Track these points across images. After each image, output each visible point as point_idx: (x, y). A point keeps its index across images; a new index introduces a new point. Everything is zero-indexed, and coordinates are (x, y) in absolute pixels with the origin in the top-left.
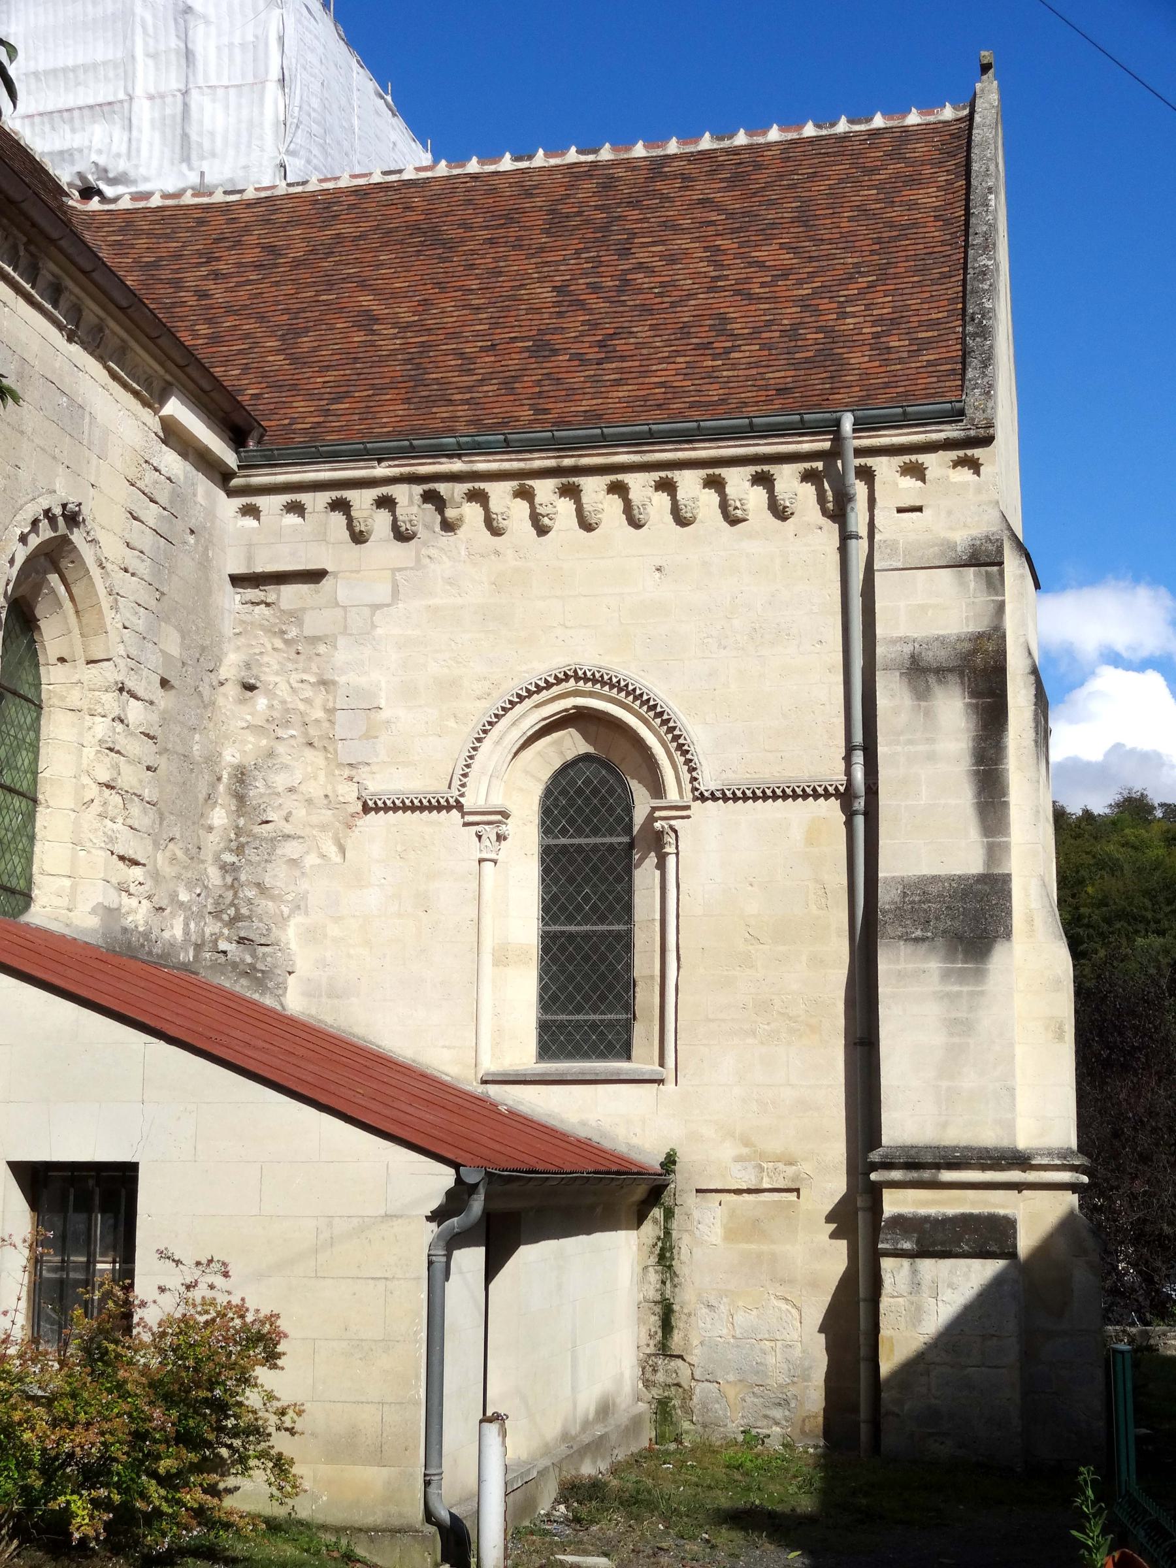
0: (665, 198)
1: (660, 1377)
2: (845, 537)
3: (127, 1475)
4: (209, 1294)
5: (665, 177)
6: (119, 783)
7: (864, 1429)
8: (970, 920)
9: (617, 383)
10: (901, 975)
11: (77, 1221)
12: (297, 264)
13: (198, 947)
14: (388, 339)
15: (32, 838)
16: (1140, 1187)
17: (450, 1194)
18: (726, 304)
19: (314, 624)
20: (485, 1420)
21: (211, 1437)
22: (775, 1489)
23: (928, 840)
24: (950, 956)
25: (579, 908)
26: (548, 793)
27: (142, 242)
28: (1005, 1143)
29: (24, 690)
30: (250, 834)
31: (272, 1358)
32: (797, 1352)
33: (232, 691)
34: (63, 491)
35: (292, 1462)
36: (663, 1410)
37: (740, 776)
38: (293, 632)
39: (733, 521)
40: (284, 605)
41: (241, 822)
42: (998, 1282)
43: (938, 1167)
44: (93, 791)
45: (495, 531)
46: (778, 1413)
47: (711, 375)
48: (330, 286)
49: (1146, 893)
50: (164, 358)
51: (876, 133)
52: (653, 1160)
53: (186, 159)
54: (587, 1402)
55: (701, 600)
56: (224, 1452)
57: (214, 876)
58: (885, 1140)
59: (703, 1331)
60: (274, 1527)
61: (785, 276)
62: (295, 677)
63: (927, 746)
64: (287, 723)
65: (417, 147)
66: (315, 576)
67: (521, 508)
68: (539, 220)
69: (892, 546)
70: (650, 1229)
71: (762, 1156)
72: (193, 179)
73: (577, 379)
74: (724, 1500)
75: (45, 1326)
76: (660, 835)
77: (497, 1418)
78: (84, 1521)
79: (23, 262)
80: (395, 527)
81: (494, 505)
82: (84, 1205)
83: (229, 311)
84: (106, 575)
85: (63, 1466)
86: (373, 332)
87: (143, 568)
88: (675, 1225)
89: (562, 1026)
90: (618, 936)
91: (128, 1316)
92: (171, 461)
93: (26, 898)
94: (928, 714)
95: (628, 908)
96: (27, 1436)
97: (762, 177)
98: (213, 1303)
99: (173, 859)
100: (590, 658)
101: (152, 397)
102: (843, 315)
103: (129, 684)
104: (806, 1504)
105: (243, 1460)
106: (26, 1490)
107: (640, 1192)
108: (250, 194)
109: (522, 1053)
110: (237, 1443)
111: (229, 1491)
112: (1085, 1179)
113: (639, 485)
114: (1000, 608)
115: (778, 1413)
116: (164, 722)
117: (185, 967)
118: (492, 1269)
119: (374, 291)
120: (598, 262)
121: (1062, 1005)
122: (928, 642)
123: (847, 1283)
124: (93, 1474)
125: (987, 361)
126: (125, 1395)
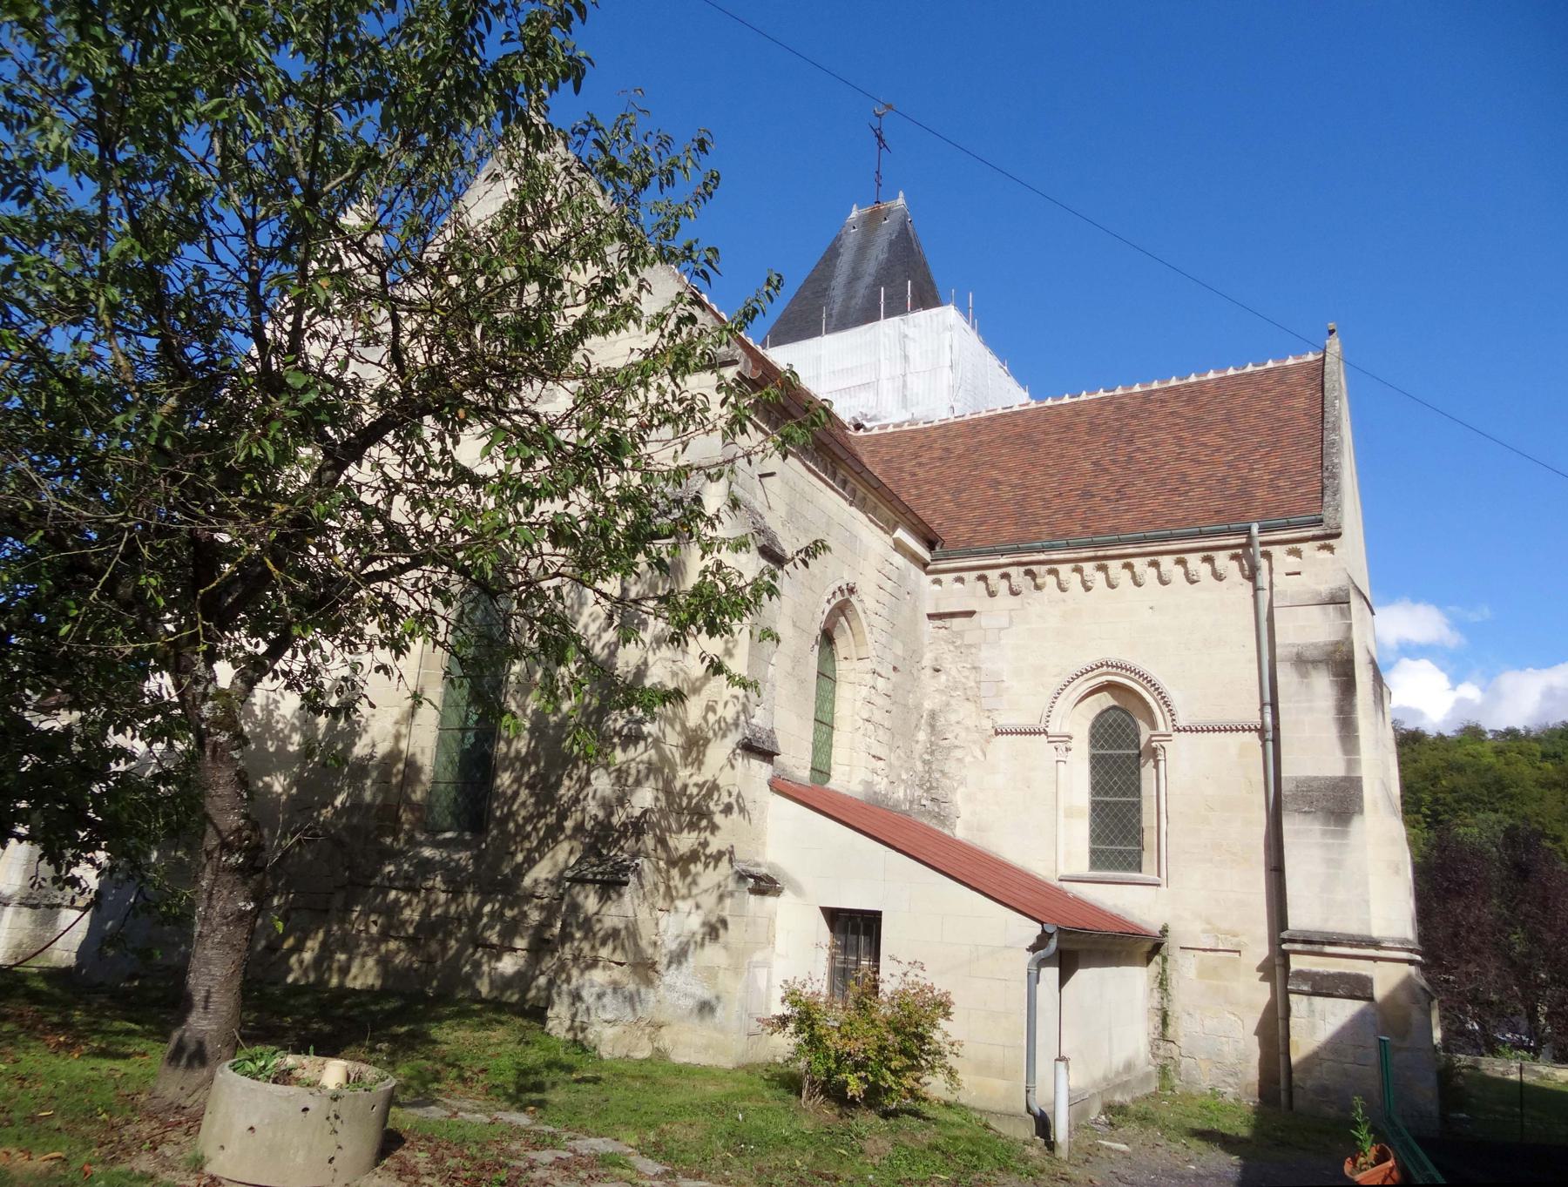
11: (852, 938)
12: (960, 457)
13: (911, 802)
14: (1006, 493)
27: (884, 450)
31: (947, 1015)
33: (928, 672)
38: (959, 643)
48: (976, 467)
50: (895, 510)
57: (919, 766)
64: (956, 689)
72: (908, 417)
78: (855, 1087)
92: (898, 559)
101: (889, 528)
103: (878, 670)
105: (932, 1068)
106: (828, 1069)
108: (936, 423)
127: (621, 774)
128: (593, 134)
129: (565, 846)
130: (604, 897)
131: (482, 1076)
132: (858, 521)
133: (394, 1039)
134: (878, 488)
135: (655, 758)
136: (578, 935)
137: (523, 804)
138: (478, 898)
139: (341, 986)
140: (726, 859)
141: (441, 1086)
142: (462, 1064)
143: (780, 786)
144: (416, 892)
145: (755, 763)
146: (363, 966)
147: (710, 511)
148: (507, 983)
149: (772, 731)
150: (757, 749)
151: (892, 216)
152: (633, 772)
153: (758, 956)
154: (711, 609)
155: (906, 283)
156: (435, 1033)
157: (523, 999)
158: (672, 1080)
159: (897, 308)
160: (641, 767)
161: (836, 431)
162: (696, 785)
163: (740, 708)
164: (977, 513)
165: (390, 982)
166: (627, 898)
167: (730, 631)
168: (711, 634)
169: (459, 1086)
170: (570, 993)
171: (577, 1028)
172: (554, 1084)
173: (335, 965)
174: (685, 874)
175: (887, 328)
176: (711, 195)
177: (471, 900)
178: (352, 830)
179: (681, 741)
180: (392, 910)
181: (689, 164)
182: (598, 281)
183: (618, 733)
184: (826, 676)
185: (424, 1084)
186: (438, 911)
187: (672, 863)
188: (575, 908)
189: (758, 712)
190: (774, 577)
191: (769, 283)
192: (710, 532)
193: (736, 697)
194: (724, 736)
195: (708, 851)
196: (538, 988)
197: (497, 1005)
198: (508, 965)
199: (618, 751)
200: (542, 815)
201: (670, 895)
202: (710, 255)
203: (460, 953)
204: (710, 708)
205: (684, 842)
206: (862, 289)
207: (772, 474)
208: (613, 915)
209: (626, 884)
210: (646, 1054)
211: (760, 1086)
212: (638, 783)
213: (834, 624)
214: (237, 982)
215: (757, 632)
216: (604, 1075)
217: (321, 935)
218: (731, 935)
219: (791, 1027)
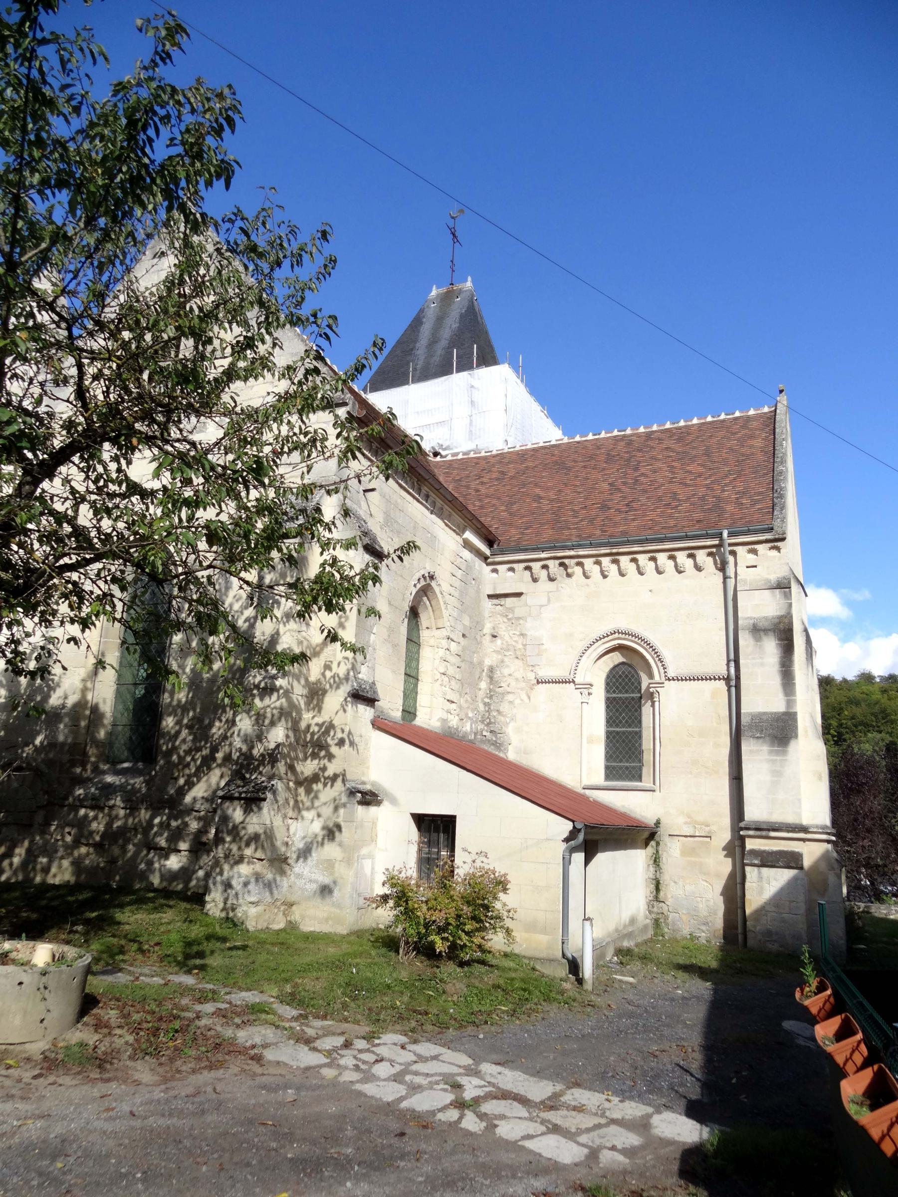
0: (653, 447)
1: (655, 910)
2: (725, 578)
5: (652, 439)
6: (448, 673)
7: (740, 937)
8: (781, 731)
9: (634, 520)
10: (751, 751)
12: (512, 478)
13: (476, 734)
14: (545, 505)
16: (866, 843)
17: (571, 832)
18: (676, 488)
19: (518, 612)
20: (585, 919)
22: (703, 958)
23: (762, 696)
24: (772, 744)
25: (621, 722)
26: (608, 677)
27: (455, 472)
28: (797, 822)
31: (505, 890)
32: (711, 903)
33: (488, 638)
34: (429, 568)
36: (657, 923)
37: (684, 671)
39: (680, 572)
42: (794, 879)
43: (769, 830)
44: (438, 676)
45: (587, 577)
46: (704, 928)
47: (670, 516)
48: (524, 485)
49: (872, 714)
50: (464, 517)
51: (736, 419)
52: (651, 822)
53: (471, 439)
54: (625, 917)
55: (669, 603)
57: (481, 707)
58: (746, 818)
59: (673, 891)
60: (506, 955)
61: (700, 476)
63: (760, 663)
64: (508, 650)
66: (519, 595)
67: (597, 568)
68: (603, 458)
69: (745, 581)
70: (650, 850)
71: (696, 822)
72: (473, 447)
73: (617, 519)
74: (681, 961)
76: (652, 694)
77: (589, 919)
78: (440, 946)
81: (586, 567)
82: (437, 830)
83: (487, 496)
84: (443, 597)
88: (660, 848)
89: (614, 768)
90: (636, 733)
91: (453, 871)
92: (467, 554)
93: (415, 715)
94: (760, 647)
95: (640, 722)
97: (690, 438)
100: (624, 626)
101: (460, 531)
102: (724, 491)
104: (714, 964)
106: (419, 933)
107: (646, 835)
108: (494, 453)
109: (599, 777)
112: (834, 838)
113: (642, 559)
114: (790, 605)
115: (704, 928)
117: (471, 741)
118: (587, 862)
119: (540, 487)
120: (626, 474)
121: (823, 768)
122: (760, 619)
123: (732, 876)
124: (441, 930)
125: (783, 507)
126: (453, 901)
127: (259, 717)
128: (239, 223)
130: (247, 810)
131: (157, 948)
133: (87, 922)
135: (285, 704)
136: (228, 839)
137: (184, 741)
140: (340, 780)
142: (141, 939)
143: (379, 724)
144: (101, 809)
145: (362, 708)
147: (327, 517)
148: (173, 876)
149: (374, 683)
150: (363, 697)
151: (463, 295)
152: (269, 715)
153: (364, 851)
156: (119, 916)
158: (301, 945)
159: (465, 365)
160: (275, 711)
162: (317, 724)
163: (350, 666)
165: (83, 876)
166: (265, 810)
168: (329, 611)
170: (222, 882)
172: (212, 952)
173: (39, 867)
174: (308, 791)
175: (458, 380)
176: (330, 274)
177: (144, 814)
178: (50, 763)
179: (305, 692)
182: (241, 338)
183: (257, 687)
184: (413, 641)
186: (118, 823)
187: (299, 783)
188: (225, 819)
189: (364, 669)
191: (375, 344)
193: (347, 658)
194: (338, 687)
195: (326, 774)
196: (198, 879)
197: (166, 894)
198: (174, 862)
199: (257, 701)
200: (199, 749)
202: (331, 321)
203: (136, 854)
204: (328, 667)
205: (308, 768)
208: (254, 824)
209: (264, 800)
210: (281, 926)
211: (367, 946)
212: (273, 724)
215: (363, 610)
216: (250, 943)
217: (26, 843)
218: (345, 836)
219: (391, 903)
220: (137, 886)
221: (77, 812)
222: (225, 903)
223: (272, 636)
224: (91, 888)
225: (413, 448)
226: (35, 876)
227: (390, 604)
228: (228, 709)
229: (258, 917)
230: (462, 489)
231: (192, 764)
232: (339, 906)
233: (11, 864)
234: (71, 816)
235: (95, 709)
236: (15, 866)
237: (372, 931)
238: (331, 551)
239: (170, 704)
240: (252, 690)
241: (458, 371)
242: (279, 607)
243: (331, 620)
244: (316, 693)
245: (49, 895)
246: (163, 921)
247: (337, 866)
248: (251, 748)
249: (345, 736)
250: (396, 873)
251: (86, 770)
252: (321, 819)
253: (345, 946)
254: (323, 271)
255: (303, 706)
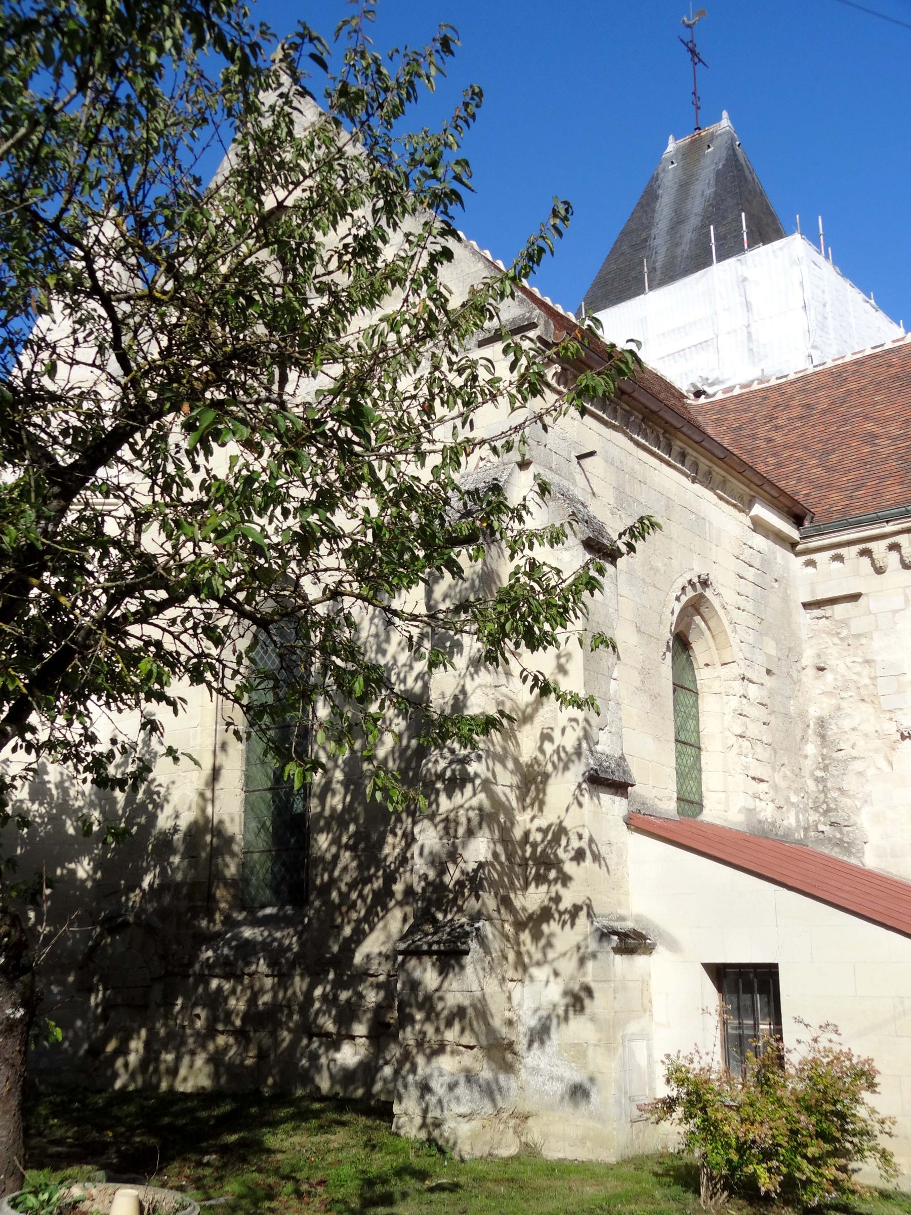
3: (788, 1155)
4: (828, 1045)
6: (747, 734)
11: (746, 998)
12: (824, 412)
13: (806, 830)
14: (885, 447)
15: (700, 770)
21: (838, 1135)
27: (731, 416)
29: (687, 685)
30: (831, 758)
31: (872, 1087)
33: (811, 672)
35: (892, 1155)
38: (844, 633)
40: (837, 617)
41: (825, 751)
48: (846, 421)
50: (749, 483)
56: (848, 1145)
57: (811, 785)
60: (885, 1196)
62: (849, 660)
64: (847, 689)
65: (894, 326)
66: (854, 597)
72: (757, 374)
75: (733, 1063)
78: (766, 1183)
79: (663, 444)
80: (902, 561)
83: (786, 447)
85: (750, 1148)
86: (875, 445)
87: (749, 606)
92: (760, 541)
93: (701, 806)
96: (726, 1129)
98: (831, 1051)
99: (785, 777)
101: (745, 505)
103: (748, 675)
105: (860, 1151)
106: (729, 1161)
108: (792, 377)
110: (856, 1140)
111: (854, 1171)
116: (771, 695)
119: (873, 419)
124: (767, 1155)
126: (782, 1106)
127: (449, 825)
128: (308, 48)
129: (397, 914)
130: (444, 970)
131: (320, 1189)
132: (704, 500)
133: (224, 1150)
134: (725, 458)
135: (487, 804)
136: (419, 1016)
137: (345, 869)
138: (307, 980)
139: (171, 1090)
140: (583, 914)
141: (274, 1204)
142: (298, 1176)
143: (638, 823)
144: (239, 978)
145: (606, 798)
146: (191, 1066)
147: (513, 500)
148: (348, 1076)
149: (622, 758)
150: (606, 781)
151: (717, 142)
152: (463, 820)
153: (633, 1028)
154: (521, 617)
155: (742, 215)
156: (272, 1140)
157: (368, 1094)
158: (542, 1182)
159: (730, 247)
160: (472, 814)
161: (672, 401)
162: (539, 830)
163: (581, 734)
164: (852, 475)
165: (223, 1080)
166: (469, 970)
167: (553, 641)
168: (533, 647)
169: (294, 1203)
170: (416, 1084)
171: (431, 1125)
172: (404, 1195)
173: (163, 1067)
174: (537, 936)
175: (722, 272)
176: (473, 116)
177: (299, 984)
178: (163, 913)
179: (515, 780)
180: (215, 1001)
181: (433, 71)
182: (349, 240)
183: (440, 776)
184: (684, 687)
185: (256, 1203)
186: (267, 998)
187: (520, 926)
188: (414, 985)
189: (603, 736)
190: (601, 571)
191: (555, 213)
192: (516, 525)
193: (575, 720)
194: (566, 768)
195: (562, 907)
196: (385, 1081)
197: (340, 1104)
198: (349, 1055)
199: (443, 798)
200: (369, 880)
201: (522, 965)
202: (458, 169)
203: (295, 1043)
204: (546, 737)
205: (532, 899)
206: (688, 233)
207: (591, 454)
208: (457, 991)
209: (467, 953)
210: (513, 1150)
211: (648, 1182)
212: (470, 833)
213: (689, 626)
214: (14, 1102)
215: (588, 641)
216: (462, 1180)
217: (143, 1033)
218: (596, 1006)
219: (679, 1111)
220: (299, 1092)
221: (207, 984)
222: (424, 1118)
223: (456, 697)
224: (234, 1097)
225: (626, 363)
226: (159, 1081)
227: (639, 631)
228: (404, 816)
229: (474, 1136)
230: (745, 442)
231: (359, 902)
232: (600, 1118)
233: (126, 1065)
234: (200, 990)
235: (218, 831)
236: (131, 1066)
237: (661, 1157)
238: (527, 551)
239: (320, 815)
240: (434, 783)
241: (720, 258)
242: (461, 651)
243: (541, 661)
244: (534, 781)
245: (175, 1108)
246: (332, 1146)
247: (590, 1053)
248: (442, 871)
249: (584, 844)
250: (682, 1061)
251: (214, 921)
252: (559, 980)
253: (611, 1183)
254: (463, 114)
255: (514, 804)
